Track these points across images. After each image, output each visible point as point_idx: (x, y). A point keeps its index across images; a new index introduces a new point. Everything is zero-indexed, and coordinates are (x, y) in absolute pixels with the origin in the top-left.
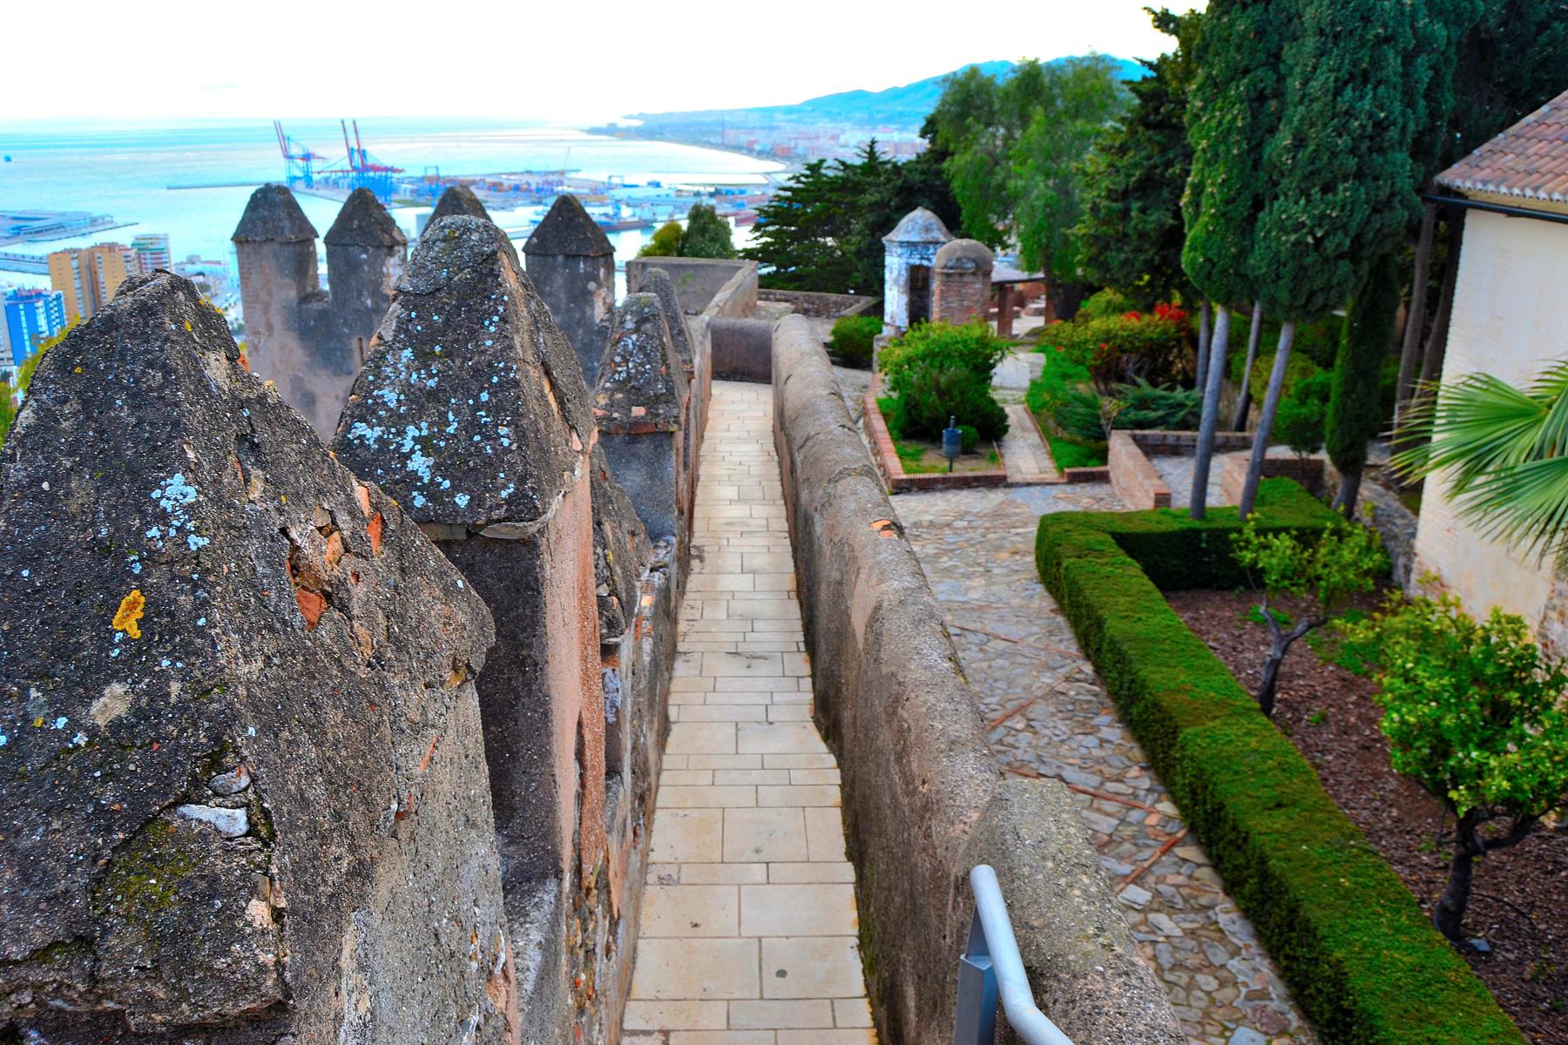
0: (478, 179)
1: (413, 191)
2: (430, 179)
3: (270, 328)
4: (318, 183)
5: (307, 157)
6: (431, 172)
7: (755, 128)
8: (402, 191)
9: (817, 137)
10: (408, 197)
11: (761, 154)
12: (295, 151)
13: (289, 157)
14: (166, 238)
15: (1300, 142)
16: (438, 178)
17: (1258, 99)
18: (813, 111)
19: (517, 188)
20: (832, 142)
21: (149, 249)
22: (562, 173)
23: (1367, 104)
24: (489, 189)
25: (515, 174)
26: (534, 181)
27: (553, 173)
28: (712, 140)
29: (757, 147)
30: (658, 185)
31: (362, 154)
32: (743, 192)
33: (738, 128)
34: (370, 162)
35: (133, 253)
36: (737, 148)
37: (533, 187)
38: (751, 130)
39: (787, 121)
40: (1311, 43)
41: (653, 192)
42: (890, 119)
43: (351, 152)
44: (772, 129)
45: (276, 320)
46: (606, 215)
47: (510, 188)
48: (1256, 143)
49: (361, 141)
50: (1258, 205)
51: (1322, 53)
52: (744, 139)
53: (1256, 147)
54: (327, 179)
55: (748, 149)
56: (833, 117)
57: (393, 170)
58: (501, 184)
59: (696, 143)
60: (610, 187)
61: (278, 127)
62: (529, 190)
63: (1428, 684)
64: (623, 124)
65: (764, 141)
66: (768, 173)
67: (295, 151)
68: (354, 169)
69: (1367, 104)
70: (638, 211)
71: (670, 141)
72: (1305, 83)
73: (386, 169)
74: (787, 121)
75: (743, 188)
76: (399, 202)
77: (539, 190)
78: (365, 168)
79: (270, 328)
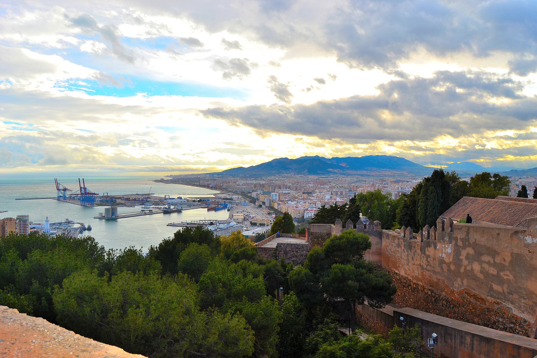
0: (121, 197)
1: (100, 201)
2: (105, 197)
3: (338, 232)
4: (68, 198)
5: (65, 190)
6: (105, 195)
7: (208, 179)
8: (97, 201)
9: (229, 183)
10: (99, 203)
11: (212, 188)
12: (61, 187)
13: (58, 190)
14: (28, 216)
15: (429, 214)
16: (108, 196)
17: (425, 210)
18: (226, 174)
19: (135, 200)
20: (234, 184)
21: (23, 221)
22: (149, 194)
23: (434, 211)
24: (125, 200)
25: (133, 195)
26: (141, 198)
27: (146, 195)
28: (196, 184)
29: (210, 186)
30: (181, 198)
31: (85, 189)
32: (209, 200)
33: (203, 180)
34: (87, 191)
35: (17, 221)
36: (204, 186)
37: (141, 199)
38: (208, 180)
39: (219, 177)
40: (430, 206)
41: (179, 201)
42: (251, 177)
43: (81, 188)
44: (215, 180)
45: (339, 231)
46: (166, 208)
47: (133, 200)
48: (426, 213)
49: (85, 185)
50: (426, 219)
51: (430, 207)
52: (206, 183)
53: (426, 214)
54: (70, 197)
55: (208, 187)
56: (233, 176)
57: (95, 194)
58: (129, 198)
59: (190, 185)
60: (166, 199)
61: (56, 180)
62: (139, 200)
63: (450, 260)
64: (166, 179)
65: (213, 184)
66: (215, 194)
67: (61, 187)
68: (81, 194)
69: (434, 211)
70: (176, 207)
71: (182, 184)
72: (429, 209)
73: (93, 194)
74: (219, 177)
75: (208, 199)
76: (96, 204)
77: (143, 200)
78: (86, 193)
79: (338, 232)
